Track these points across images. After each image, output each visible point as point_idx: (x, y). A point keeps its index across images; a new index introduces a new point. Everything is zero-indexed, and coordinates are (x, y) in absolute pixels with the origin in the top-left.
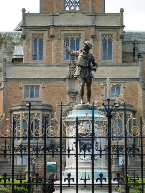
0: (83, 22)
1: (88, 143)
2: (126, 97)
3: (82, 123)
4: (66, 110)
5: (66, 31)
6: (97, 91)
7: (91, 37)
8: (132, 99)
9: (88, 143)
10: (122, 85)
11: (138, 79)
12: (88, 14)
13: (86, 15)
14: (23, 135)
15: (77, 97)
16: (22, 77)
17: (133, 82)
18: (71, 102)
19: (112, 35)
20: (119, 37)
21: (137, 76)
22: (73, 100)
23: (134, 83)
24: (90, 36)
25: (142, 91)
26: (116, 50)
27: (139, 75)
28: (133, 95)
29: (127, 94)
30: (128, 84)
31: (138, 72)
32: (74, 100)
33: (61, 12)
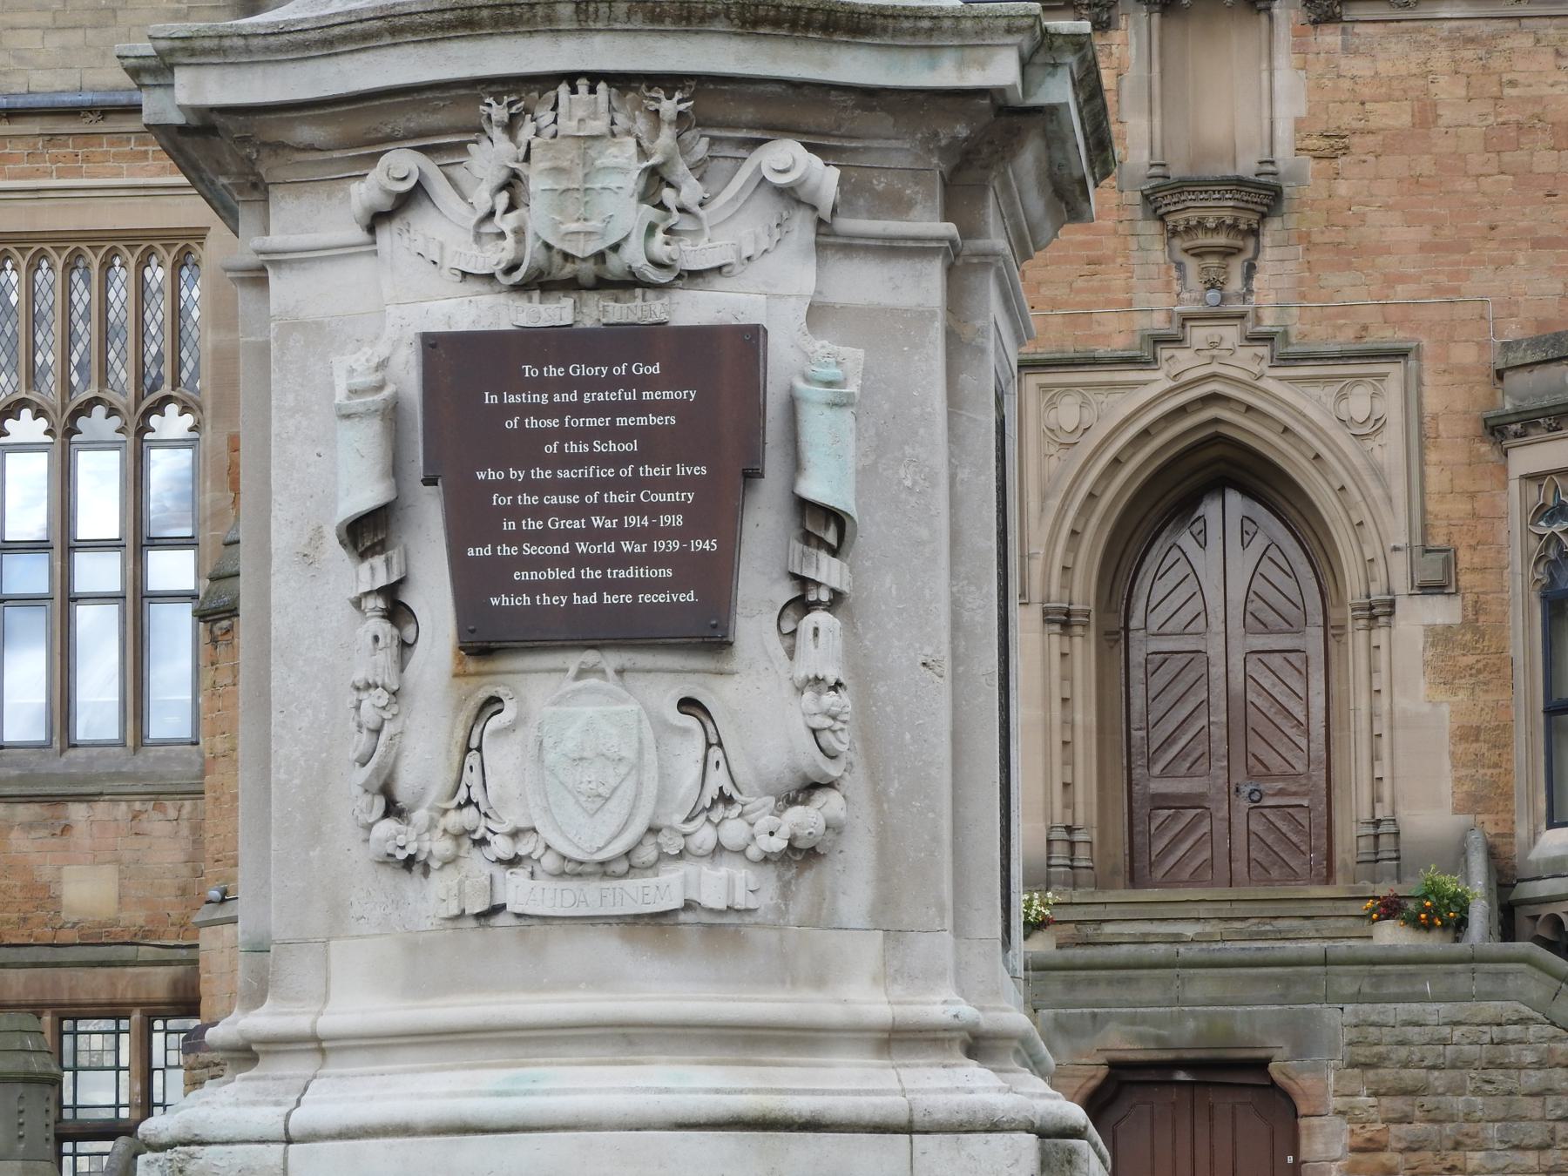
1: (636, 535)
3: (511, 127)
4: (1127, 421)
9: (636, 535)
15: (1266, 240)
18: (1186, 319)
22: (1212, 285)
32: (1235, 284)
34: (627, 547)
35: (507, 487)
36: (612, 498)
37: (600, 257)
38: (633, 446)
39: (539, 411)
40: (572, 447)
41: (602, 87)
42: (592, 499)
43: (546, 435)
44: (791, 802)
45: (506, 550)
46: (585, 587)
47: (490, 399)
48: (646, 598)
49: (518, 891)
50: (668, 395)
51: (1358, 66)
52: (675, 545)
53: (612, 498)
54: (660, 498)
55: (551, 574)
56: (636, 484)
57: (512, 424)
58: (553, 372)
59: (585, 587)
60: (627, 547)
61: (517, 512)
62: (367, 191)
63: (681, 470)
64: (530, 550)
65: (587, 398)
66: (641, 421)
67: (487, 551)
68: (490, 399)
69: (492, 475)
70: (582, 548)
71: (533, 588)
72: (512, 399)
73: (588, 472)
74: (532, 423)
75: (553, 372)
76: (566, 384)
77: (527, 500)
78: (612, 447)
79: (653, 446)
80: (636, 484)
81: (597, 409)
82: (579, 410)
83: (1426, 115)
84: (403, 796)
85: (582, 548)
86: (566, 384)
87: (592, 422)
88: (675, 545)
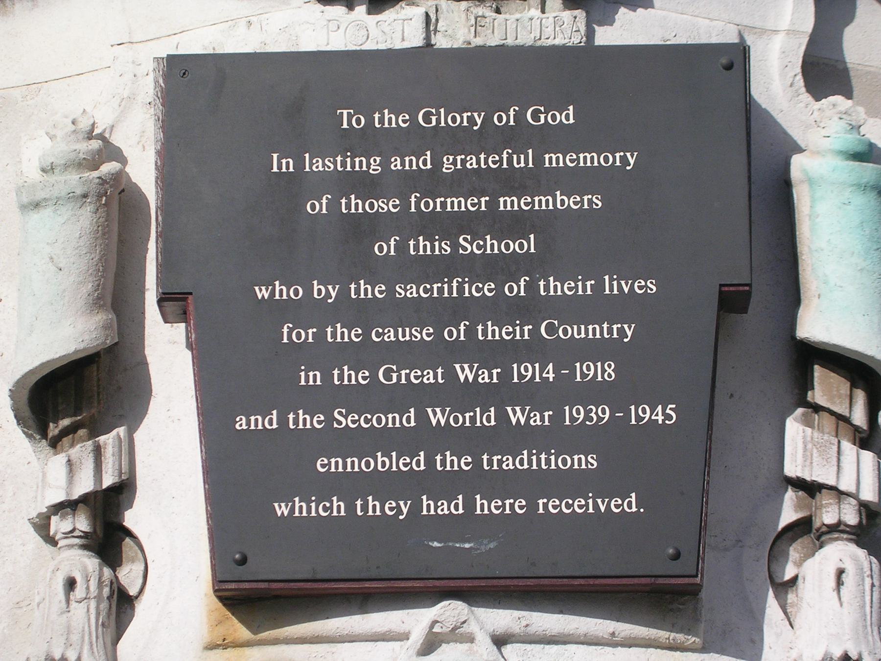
34: (517, 416)
36: (491, 331)
38: (530, 245)
40: (421, 246)
47: (286, 165)
48: (552, 505)
50: (588, 159)
52: (602, 413)
53: (491, 331)
54: (576, 332)
55: (381, 462)
60: (517, 416)
63: (611, 286)
64: (344, 420)
66: (542, 202)
67: (272, 422)
70: (437, 417)
72: (318, 165)
73: (450, 288)
74: (355, 205)
78: (492, 245)
85: (437, 417)
87: (456, 204)
88: (602, 413)
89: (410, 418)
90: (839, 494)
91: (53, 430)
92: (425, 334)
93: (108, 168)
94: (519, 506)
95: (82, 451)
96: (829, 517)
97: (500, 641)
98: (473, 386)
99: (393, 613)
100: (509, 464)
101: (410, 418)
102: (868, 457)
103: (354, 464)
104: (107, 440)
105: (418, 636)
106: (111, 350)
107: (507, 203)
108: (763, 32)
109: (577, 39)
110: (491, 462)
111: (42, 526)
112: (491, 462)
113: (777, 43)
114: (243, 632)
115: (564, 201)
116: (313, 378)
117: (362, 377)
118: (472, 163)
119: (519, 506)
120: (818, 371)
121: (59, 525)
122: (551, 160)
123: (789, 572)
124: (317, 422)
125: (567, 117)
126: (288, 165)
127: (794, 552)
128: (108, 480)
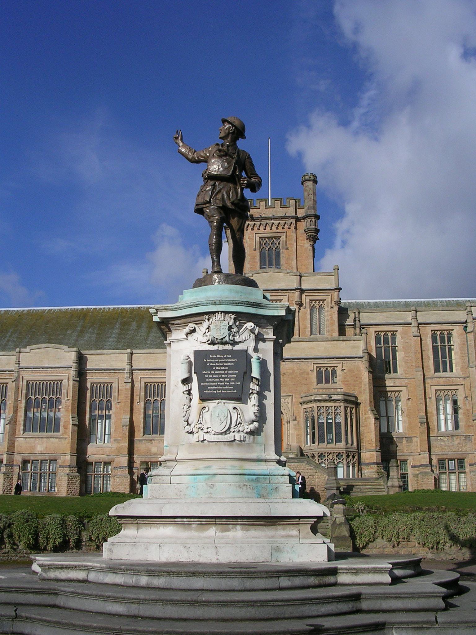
0: (284, 285)
1: (227, 382)
2: (346, 383)
3: (209, 320)
5: (312, 297)
6: (306, 376)
7: (296, 304)
8: (354, 386)
9: (227, 382)
10: (340, 366)
11: (362, 358)
12: (291, 274)
13: (288, 275)
14: (126, 442)
16: (93, 367)
17: (355, 363)
19: (323, 300)
20: (333, 303)
21: (361, 354)
23: (356, 363)
24: (295, 303)
25: (367, 374)
26: (330, 320)
27: (363, 353)
28: (355, 381)
29: (346, 380)
30: (347, 364)
31: (362, 349)
33: (254, 272)
34: (226, 383)
35: (207, 374)
36: (223, 376)
37: (222, 339)
38: (227, 368)
39: (212, 362)
40: (217, 368)
41: (223, 313)
42: (220, 376)
43: (213, 366)
44: (250, 424)
45: (207, 384)
46: (219, 390)
47: (205, 360)
48: (228, 391)
49: (207, 437)
50: (232, 360)
51: (287, 366)
52: (233, 383)
53: (223, 376)
56: (227, 374)
57: (208, 364)
58: (214, 356)
59: (219, 390)
60: (226, 383)
61: (209, 378)
62: (187, 330)
63: (234, 372)
64: (210, 384)
65: (220, 361)
66: (228, 364)
67: (204, 384)
68: (205, 360)
69: (205, 372)
70: (219, 384)
71: (211, 390)
72: (208, 361)
73: (220, 372)
74: (211, 364)
75: (214, 356)
76: (217, 358)
77: (210, 376)
79: (230, 368)
80: (227, 374)
81: (221, 362)
82: (218, 362)
83: (293, 371)
84: (190, 422)
85: (219, 384)
86: (217, 358)
87: (221, 364)
88: (233, 383)
89: (216, 384)
90: (255, 390)
91: (184, 384)
92: (218, 376)
93: (189, 360)
94: (226, 391)
95: (187, 386)
96: (254, 392)
97: (224, 403)
98: (222, 381)
99: (296, 514)
100: (225, 388)
101: (216, 384)
102: (258, 387)
103: (211, 388)
104: (189, 385)
105: (217, 403)
106: (189, 377)
107: (225, 364)
108: (250, 346)
109: (232, 349)
110: (223, 388)
111: (183, 392)
112: (223, 388)
113: (251, 347)
114: (202, 402)
115: (230, 364)
116: (208, 380)
117: (212, 380)
118: (222, 360)
119: (226, 391)
120: (254, 379)
121: (185, 392)
122: (229, 360)
123: (250, 397)
124: (208, 384)
125: (230, 356)
126: (205, 361)
127: (251, 395)
128: (189, 389)
